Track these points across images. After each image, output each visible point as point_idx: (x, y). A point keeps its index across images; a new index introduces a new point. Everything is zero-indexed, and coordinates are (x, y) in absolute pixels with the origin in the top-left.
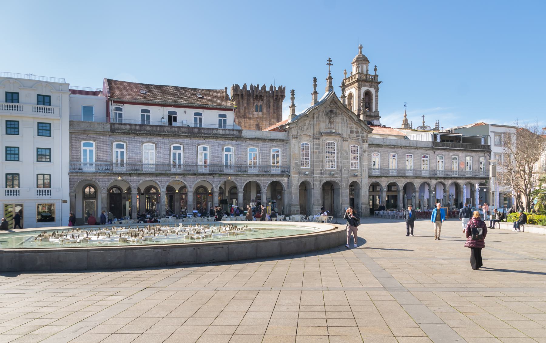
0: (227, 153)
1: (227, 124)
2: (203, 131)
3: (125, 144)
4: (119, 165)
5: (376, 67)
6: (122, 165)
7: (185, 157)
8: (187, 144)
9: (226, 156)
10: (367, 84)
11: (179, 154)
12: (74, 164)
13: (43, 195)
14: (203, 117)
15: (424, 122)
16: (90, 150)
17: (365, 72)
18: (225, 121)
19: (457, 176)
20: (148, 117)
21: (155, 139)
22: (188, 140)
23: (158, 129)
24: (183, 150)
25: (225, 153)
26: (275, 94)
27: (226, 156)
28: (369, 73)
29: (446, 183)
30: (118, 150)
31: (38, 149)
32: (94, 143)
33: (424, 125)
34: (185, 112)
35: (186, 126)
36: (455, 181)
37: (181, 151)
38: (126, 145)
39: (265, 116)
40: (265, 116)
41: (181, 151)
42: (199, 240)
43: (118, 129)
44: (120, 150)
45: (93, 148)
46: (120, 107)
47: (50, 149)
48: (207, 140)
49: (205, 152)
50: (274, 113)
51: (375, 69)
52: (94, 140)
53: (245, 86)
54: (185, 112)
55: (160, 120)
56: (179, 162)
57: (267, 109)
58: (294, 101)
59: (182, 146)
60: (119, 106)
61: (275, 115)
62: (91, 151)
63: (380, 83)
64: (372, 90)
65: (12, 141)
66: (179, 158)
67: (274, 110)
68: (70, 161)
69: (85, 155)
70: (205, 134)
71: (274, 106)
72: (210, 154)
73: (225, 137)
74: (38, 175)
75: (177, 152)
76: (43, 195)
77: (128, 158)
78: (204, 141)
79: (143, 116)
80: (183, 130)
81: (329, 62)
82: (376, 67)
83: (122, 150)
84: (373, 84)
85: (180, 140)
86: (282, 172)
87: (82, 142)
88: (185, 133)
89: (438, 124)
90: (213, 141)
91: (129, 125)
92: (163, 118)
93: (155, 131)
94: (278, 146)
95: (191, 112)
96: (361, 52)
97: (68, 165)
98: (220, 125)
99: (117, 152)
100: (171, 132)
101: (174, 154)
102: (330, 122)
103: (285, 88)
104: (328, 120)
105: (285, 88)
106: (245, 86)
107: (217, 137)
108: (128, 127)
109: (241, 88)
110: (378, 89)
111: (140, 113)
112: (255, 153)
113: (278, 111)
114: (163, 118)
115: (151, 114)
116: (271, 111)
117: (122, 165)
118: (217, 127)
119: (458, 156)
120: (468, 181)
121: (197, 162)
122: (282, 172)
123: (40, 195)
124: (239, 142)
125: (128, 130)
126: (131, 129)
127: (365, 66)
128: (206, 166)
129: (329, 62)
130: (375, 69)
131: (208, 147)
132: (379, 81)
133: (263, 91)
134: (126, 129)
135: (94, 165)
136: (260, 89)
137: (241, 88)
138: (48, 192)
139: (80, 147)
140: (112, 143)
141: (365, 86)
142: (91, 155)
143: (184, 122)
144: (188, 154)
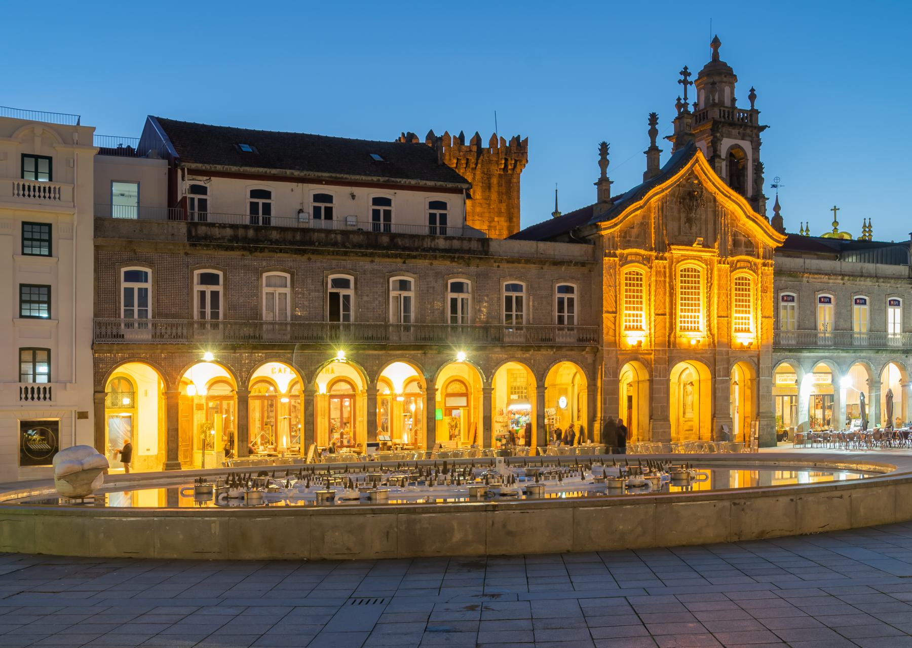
0: (454, 295)
1: (449, 223)
2: (400, 242)
3: (221, 274)
5: (752, 90)
7: (358, 305)
8: (365, 272)
9: (454, 301)
10: (735, 132)
12: (106, 325)
13: (33, 398)
15: (836, 223)
16: (140, 290)
17: (727, 102)
18: (443, 218)
20: (267, 208)
21: (289, 259)
22: (364, 264)
23: (298, 237)
24: (356, 288)
25: (451, 295)
27: (454, 301)
28: (738, 105)
30: (203, 288)
31: (22, 286)
32: (149, 271)
34: (353, 197)
35: (355, 228)
38: (225, 276)
39: (478, 209)
40: (478, 209)
41: (350, 292)
43: (206, 237)
44: (209, 289)
45: (148, 285)
46: (202, 183)
47: (49, 287)
48: (411, 263)
49: (405, 294)
50: (501, 202)
51: (752, 97)
52: (150, 264)
53: (477, 139)
54: (353, 197)
55: (294, 215)
57: (483, 192)
58: (608, 170)
59: (351, 278)
60: (201, 181)
61: (503, 207)
62: (215, 295)
63: (763, 128)
64: (746, 145)
65: (36, 269)
67: (499, 193)
68: (96, 315)
69: (129, 302)
70: (404, 249)
71: (500, 185)
72: (416, 297)
73: (450, 254)
74: (21, 349)
76: (33, 398)
78: (404, 267)
80: (356, 239)
81: (682, 78)
82: (752, 90)
83: (214, 288)
84: (748, 131)
85: (348, 262)
86: (580, 340)
87: (123, 270)
88: (360, 246)
89: (870, 226)
90: (422, 263)
91: (233, 226)
92: (301, 211)
93: (291, 243)
94: (572, 278)
95: (366, 195)
96: (716, 56)
97: (90, 325)
98: (433, 230)
100: (326, 245)
101: (203, 294)
102: (689, 221)
103: (526, 141)
104: (683, 215)
105: (526, 141)
106: (477, 139)
107: (434, 253)
108: (229, 232)
110: (760, 144)
113: (509, 198)
114: (301, 211)
115: (273, 202)
116: (494, 196)
118: (247, 221)
121: (386, 319)
122: (580, 340)
123: (26, 398)
124: (483, 268)
125: (230, 241)
126: (235, 238)
127: (727, 90)
128: (407, 328)
129: (682, 78)
130: (752, 97)
131: (505, 283)
132: (761, 123)
133: (475, 148)
134: (223, 238)
135: (150, 326)
136: (467, 143)
138: (45, 393)
139: (117, 282)
140: (261, 275)
141: (729, 136)
142: (143, 302)
143: (351, 220)
144: (365, 298)
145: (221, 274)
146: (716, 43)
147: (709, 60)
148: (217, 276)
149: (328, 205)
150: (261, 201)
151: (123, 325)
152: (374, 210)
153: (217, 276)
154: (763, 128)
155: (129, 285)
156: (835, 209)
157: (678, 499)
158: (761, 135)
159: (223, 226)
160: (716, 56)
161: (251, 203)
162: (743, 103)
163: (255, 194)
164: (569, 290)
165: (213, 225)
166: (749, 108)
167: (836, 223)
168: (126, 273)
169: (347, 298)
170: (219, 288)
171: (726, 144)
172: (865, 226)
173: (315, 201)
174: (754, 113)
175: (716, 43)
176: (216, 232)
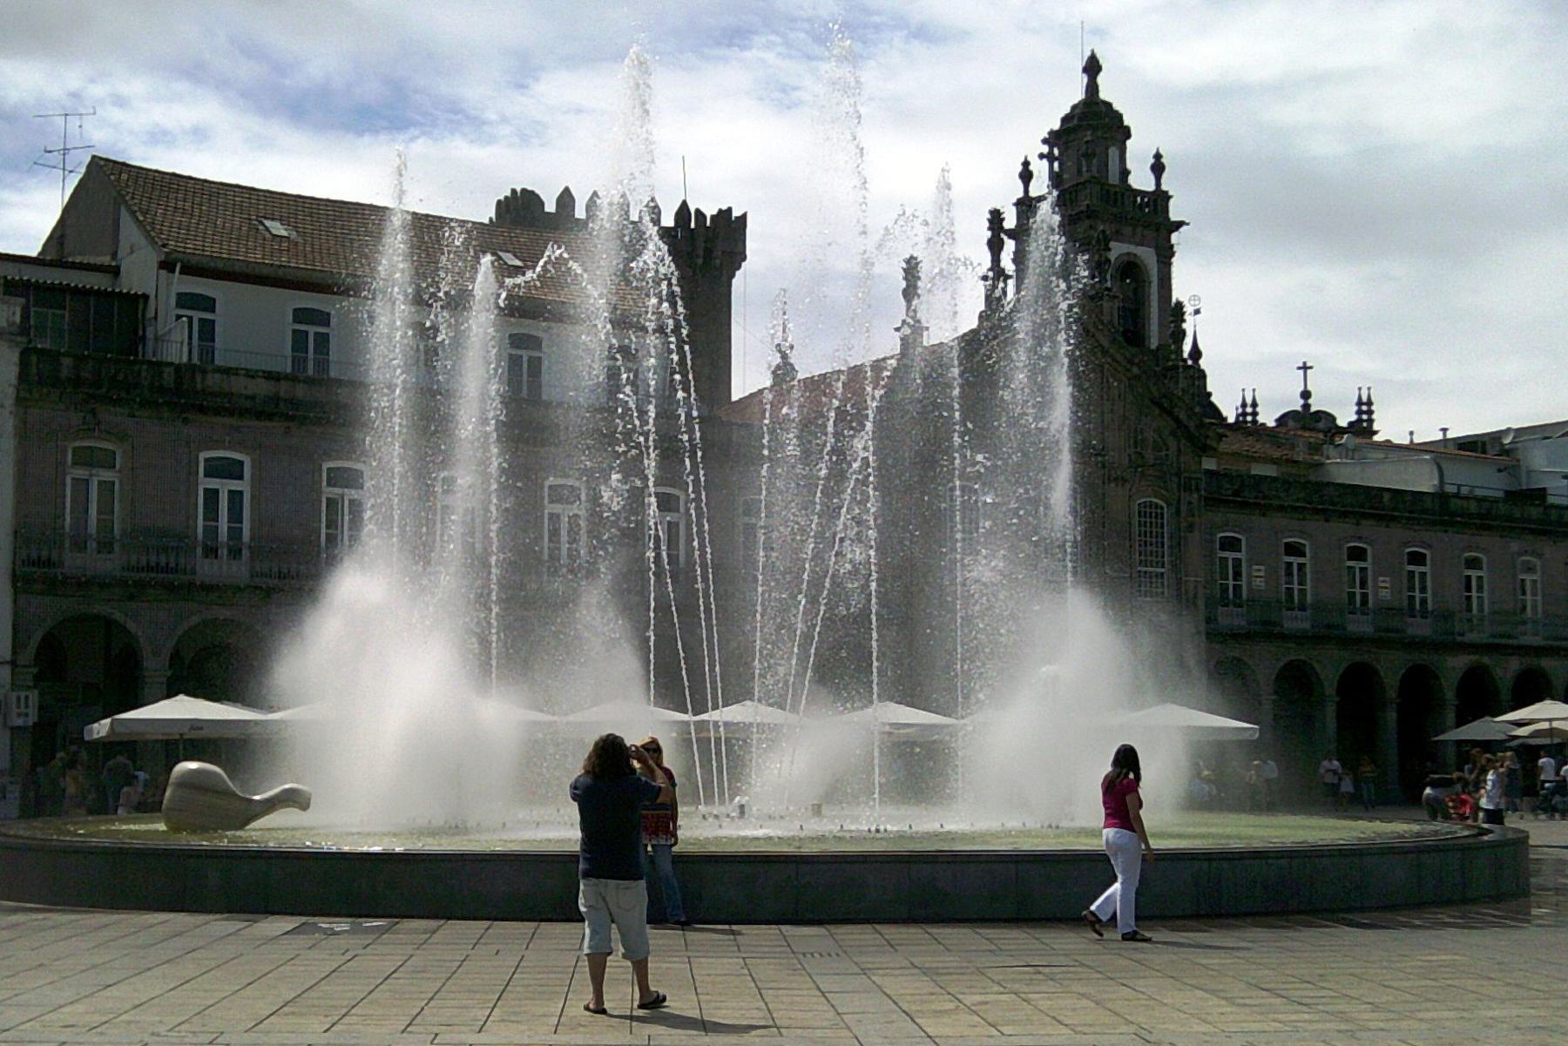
4: (224, 552)
5: (1158, 156)
6: (106, 546)
11: (235, 496)
14: (219, 317)
15: (1306, 395)
17: (1113, 178)
19: (1537, 641)
26: (701, 244)
29: (1498, 672)
32: (246, 459)
33: (1306, 406)
36: (1529, 661)
37: (243, 486)
42: (1369, 834)
51: (1158, 168)
56: (235, 533)
62: (235, 496)
63: (1179, 225)
64: (1147, 255)
66: (236, 514)
75: (225, 486)
77: (1492, 603)
79: (299, 339)
82: (1158, 156)
87: (203, 456)
89: (1369, 403)
96: (1092, 88)
99: (1289, 565)
105: (744, 216)
109: (550, 207)
111: (289, 326)
112: (1238, 555)
117: (106, 546)
119: (1540, 556)
120: (1474, 658)
130: (1158, 168)
137: (550, 207)
145: (246, 459)
146: (1093, 67)
147: (1078, 95)
148: (1365, 550)
149: (535, 354)
150: (312, 330)
151: (199, 551)
152: (294, 331)
153: (1239, 540)
154: (1179, 225)
155: (213, 483)
156: (1305, 368)
157: (1493, 845)
158: (1174, 237)
159: (251, 375)
160: (1092, 88)
161: (294, 331)
162: (1140, 179)
163: (301, 315)
164: (232, 470)
165: (227, 371)
166: (1151, 187)
167: (1306, 395)
168: (206, 460)
169: (1423, 574)
170: (243, 486)
171: (1117, 250)
172: (1360, 403)
173: (295, 321)
174: (1160, 199)
175: (1093, 67)
176: (239, 385)
